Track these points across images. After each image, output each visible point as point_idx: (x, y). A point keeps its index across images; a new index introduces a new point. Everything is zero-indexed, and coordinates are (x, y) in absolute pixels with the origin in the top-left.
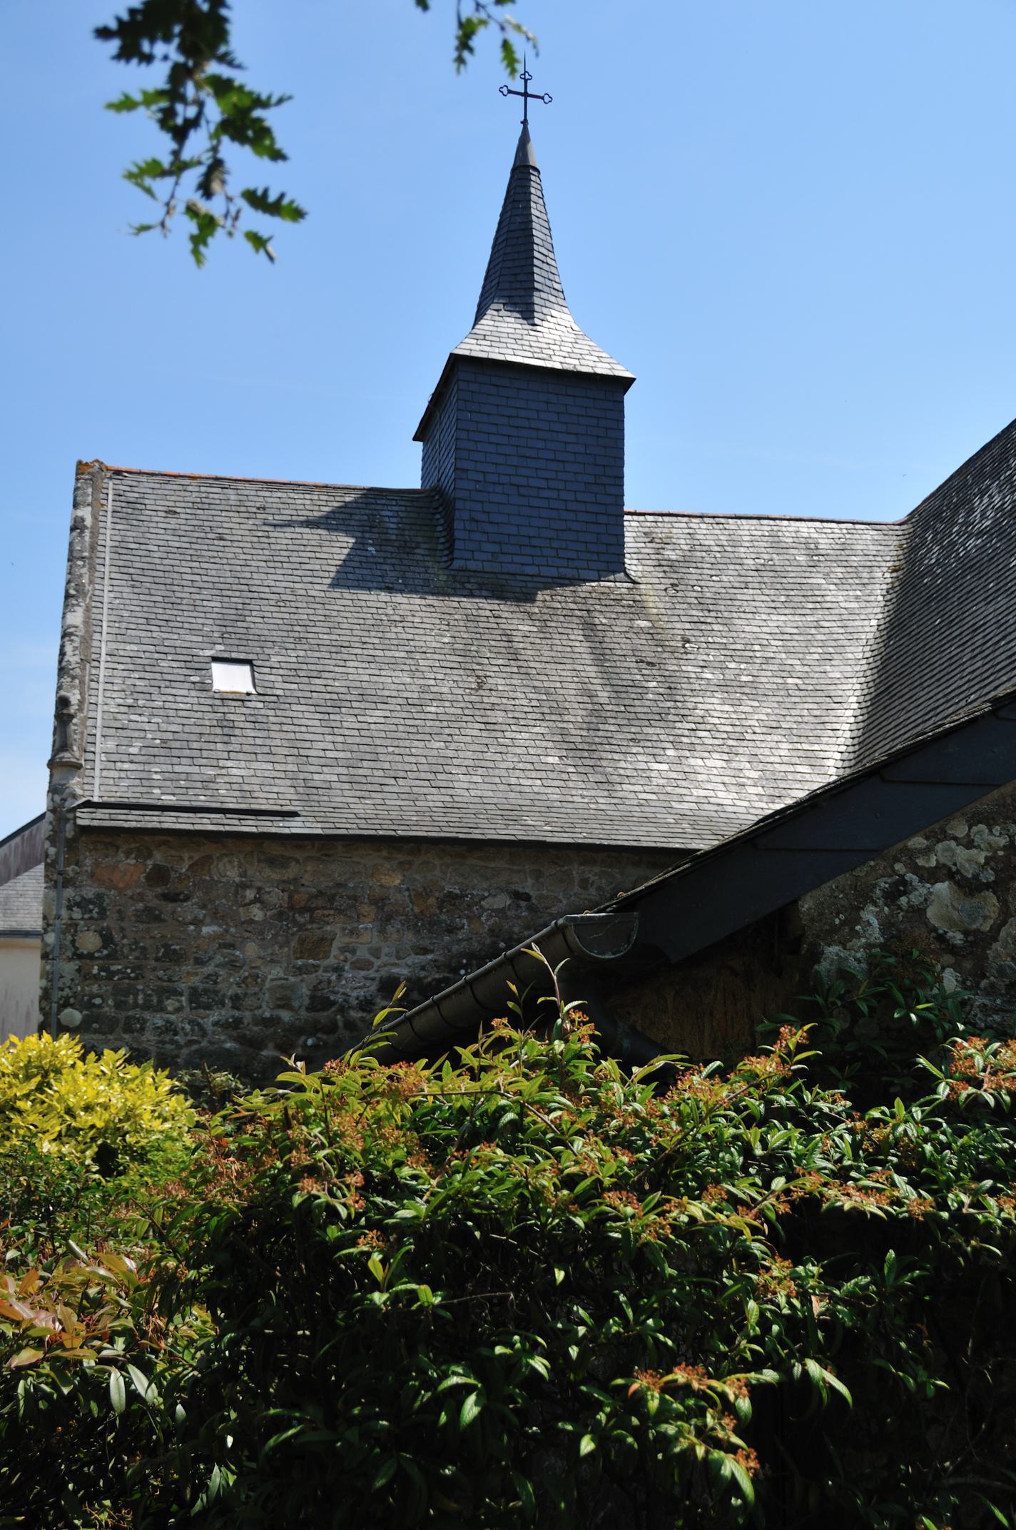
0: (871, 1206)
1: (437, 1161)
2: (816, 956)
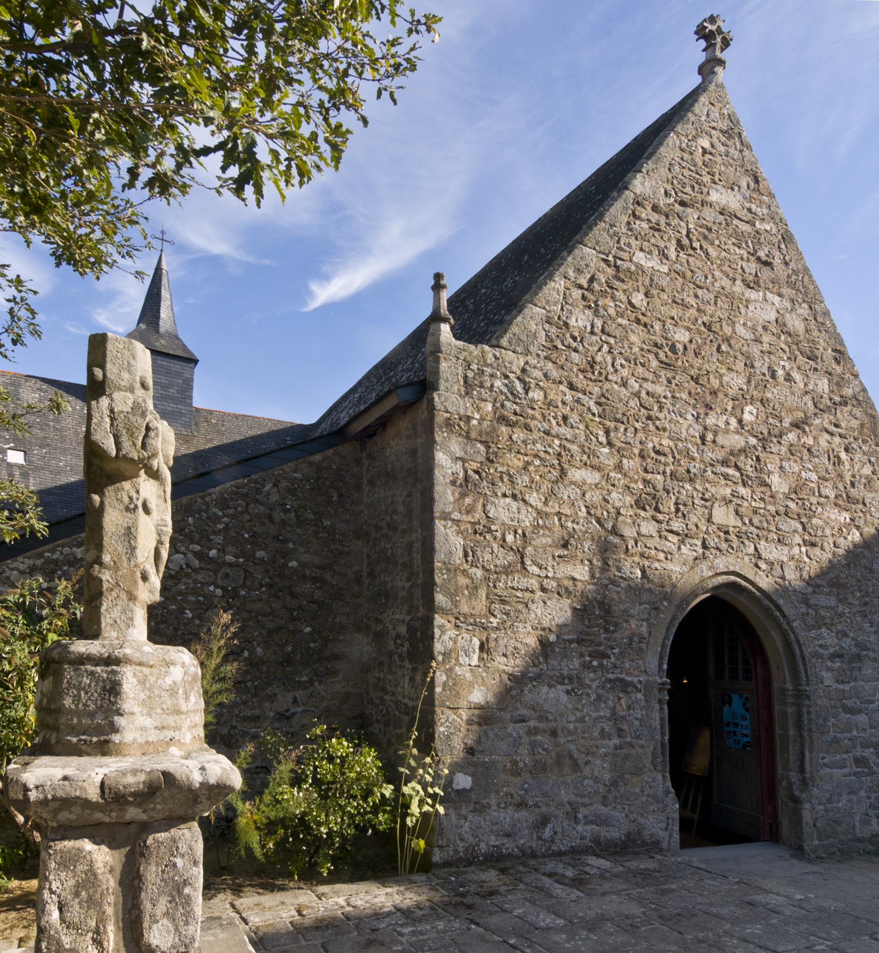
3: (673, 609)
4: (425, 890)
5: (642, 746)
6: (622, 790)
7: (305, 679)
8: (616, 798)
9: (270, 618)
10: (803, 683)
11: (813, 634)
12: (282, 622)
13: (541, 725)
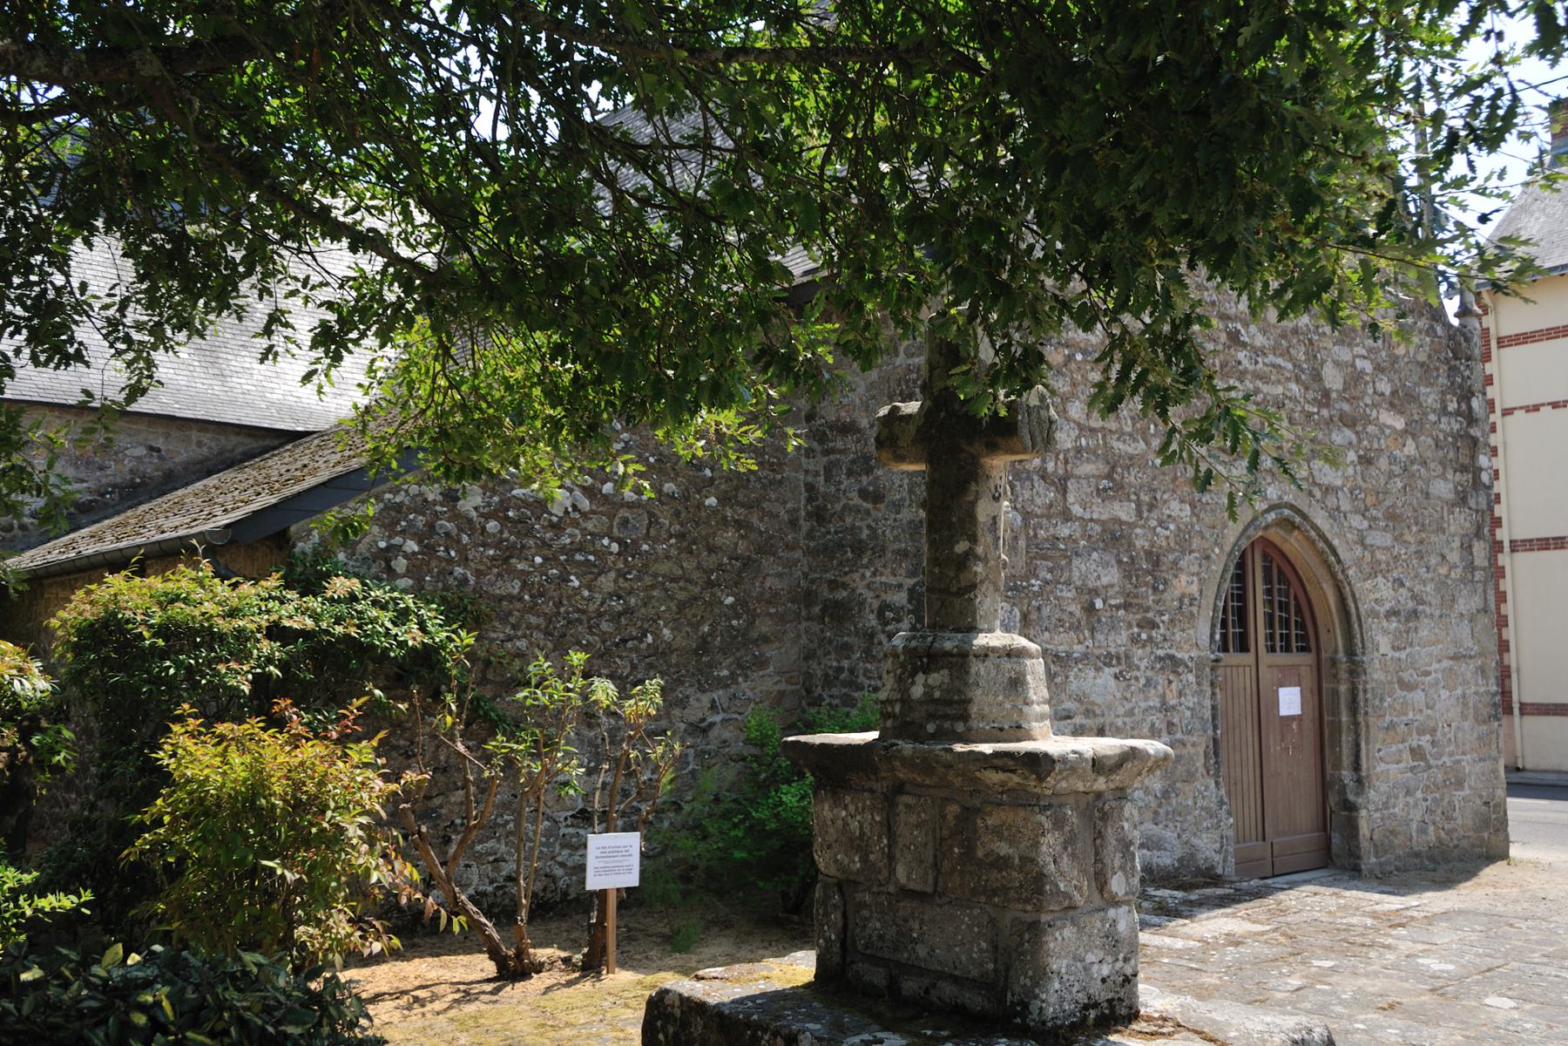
0: (296, 626)
1: (164, 609)
2: (294, 546)
3: (1224, 558)
4: (1465, 843)
5: (1194, 745)
6: (1174, 802)
7: (725, 672)
8: (1167, 813)
9: (681, 584)
10: (1359, 651)
11: (1368, 584)
12: (697, 590)
13: (1088, 722)
